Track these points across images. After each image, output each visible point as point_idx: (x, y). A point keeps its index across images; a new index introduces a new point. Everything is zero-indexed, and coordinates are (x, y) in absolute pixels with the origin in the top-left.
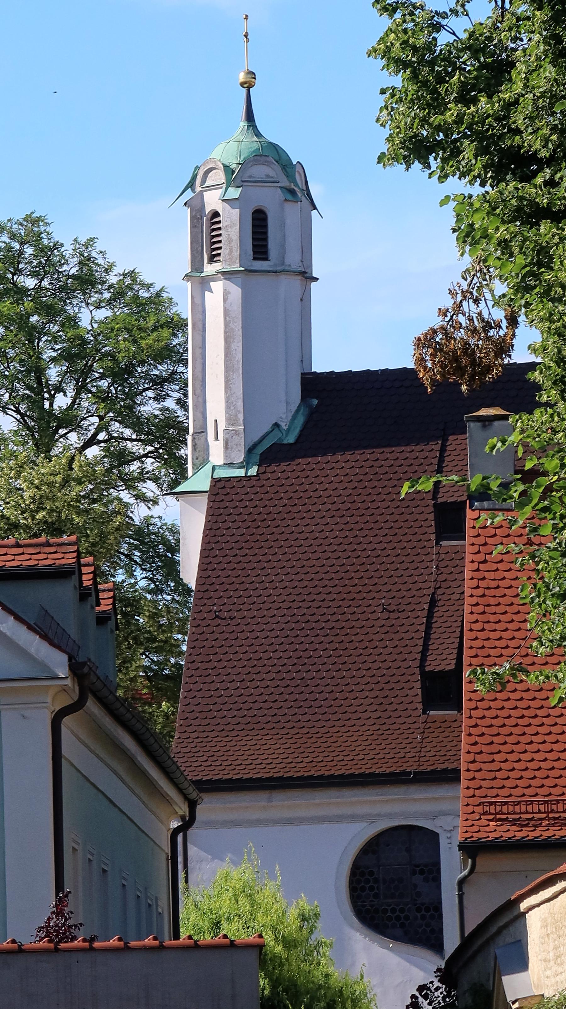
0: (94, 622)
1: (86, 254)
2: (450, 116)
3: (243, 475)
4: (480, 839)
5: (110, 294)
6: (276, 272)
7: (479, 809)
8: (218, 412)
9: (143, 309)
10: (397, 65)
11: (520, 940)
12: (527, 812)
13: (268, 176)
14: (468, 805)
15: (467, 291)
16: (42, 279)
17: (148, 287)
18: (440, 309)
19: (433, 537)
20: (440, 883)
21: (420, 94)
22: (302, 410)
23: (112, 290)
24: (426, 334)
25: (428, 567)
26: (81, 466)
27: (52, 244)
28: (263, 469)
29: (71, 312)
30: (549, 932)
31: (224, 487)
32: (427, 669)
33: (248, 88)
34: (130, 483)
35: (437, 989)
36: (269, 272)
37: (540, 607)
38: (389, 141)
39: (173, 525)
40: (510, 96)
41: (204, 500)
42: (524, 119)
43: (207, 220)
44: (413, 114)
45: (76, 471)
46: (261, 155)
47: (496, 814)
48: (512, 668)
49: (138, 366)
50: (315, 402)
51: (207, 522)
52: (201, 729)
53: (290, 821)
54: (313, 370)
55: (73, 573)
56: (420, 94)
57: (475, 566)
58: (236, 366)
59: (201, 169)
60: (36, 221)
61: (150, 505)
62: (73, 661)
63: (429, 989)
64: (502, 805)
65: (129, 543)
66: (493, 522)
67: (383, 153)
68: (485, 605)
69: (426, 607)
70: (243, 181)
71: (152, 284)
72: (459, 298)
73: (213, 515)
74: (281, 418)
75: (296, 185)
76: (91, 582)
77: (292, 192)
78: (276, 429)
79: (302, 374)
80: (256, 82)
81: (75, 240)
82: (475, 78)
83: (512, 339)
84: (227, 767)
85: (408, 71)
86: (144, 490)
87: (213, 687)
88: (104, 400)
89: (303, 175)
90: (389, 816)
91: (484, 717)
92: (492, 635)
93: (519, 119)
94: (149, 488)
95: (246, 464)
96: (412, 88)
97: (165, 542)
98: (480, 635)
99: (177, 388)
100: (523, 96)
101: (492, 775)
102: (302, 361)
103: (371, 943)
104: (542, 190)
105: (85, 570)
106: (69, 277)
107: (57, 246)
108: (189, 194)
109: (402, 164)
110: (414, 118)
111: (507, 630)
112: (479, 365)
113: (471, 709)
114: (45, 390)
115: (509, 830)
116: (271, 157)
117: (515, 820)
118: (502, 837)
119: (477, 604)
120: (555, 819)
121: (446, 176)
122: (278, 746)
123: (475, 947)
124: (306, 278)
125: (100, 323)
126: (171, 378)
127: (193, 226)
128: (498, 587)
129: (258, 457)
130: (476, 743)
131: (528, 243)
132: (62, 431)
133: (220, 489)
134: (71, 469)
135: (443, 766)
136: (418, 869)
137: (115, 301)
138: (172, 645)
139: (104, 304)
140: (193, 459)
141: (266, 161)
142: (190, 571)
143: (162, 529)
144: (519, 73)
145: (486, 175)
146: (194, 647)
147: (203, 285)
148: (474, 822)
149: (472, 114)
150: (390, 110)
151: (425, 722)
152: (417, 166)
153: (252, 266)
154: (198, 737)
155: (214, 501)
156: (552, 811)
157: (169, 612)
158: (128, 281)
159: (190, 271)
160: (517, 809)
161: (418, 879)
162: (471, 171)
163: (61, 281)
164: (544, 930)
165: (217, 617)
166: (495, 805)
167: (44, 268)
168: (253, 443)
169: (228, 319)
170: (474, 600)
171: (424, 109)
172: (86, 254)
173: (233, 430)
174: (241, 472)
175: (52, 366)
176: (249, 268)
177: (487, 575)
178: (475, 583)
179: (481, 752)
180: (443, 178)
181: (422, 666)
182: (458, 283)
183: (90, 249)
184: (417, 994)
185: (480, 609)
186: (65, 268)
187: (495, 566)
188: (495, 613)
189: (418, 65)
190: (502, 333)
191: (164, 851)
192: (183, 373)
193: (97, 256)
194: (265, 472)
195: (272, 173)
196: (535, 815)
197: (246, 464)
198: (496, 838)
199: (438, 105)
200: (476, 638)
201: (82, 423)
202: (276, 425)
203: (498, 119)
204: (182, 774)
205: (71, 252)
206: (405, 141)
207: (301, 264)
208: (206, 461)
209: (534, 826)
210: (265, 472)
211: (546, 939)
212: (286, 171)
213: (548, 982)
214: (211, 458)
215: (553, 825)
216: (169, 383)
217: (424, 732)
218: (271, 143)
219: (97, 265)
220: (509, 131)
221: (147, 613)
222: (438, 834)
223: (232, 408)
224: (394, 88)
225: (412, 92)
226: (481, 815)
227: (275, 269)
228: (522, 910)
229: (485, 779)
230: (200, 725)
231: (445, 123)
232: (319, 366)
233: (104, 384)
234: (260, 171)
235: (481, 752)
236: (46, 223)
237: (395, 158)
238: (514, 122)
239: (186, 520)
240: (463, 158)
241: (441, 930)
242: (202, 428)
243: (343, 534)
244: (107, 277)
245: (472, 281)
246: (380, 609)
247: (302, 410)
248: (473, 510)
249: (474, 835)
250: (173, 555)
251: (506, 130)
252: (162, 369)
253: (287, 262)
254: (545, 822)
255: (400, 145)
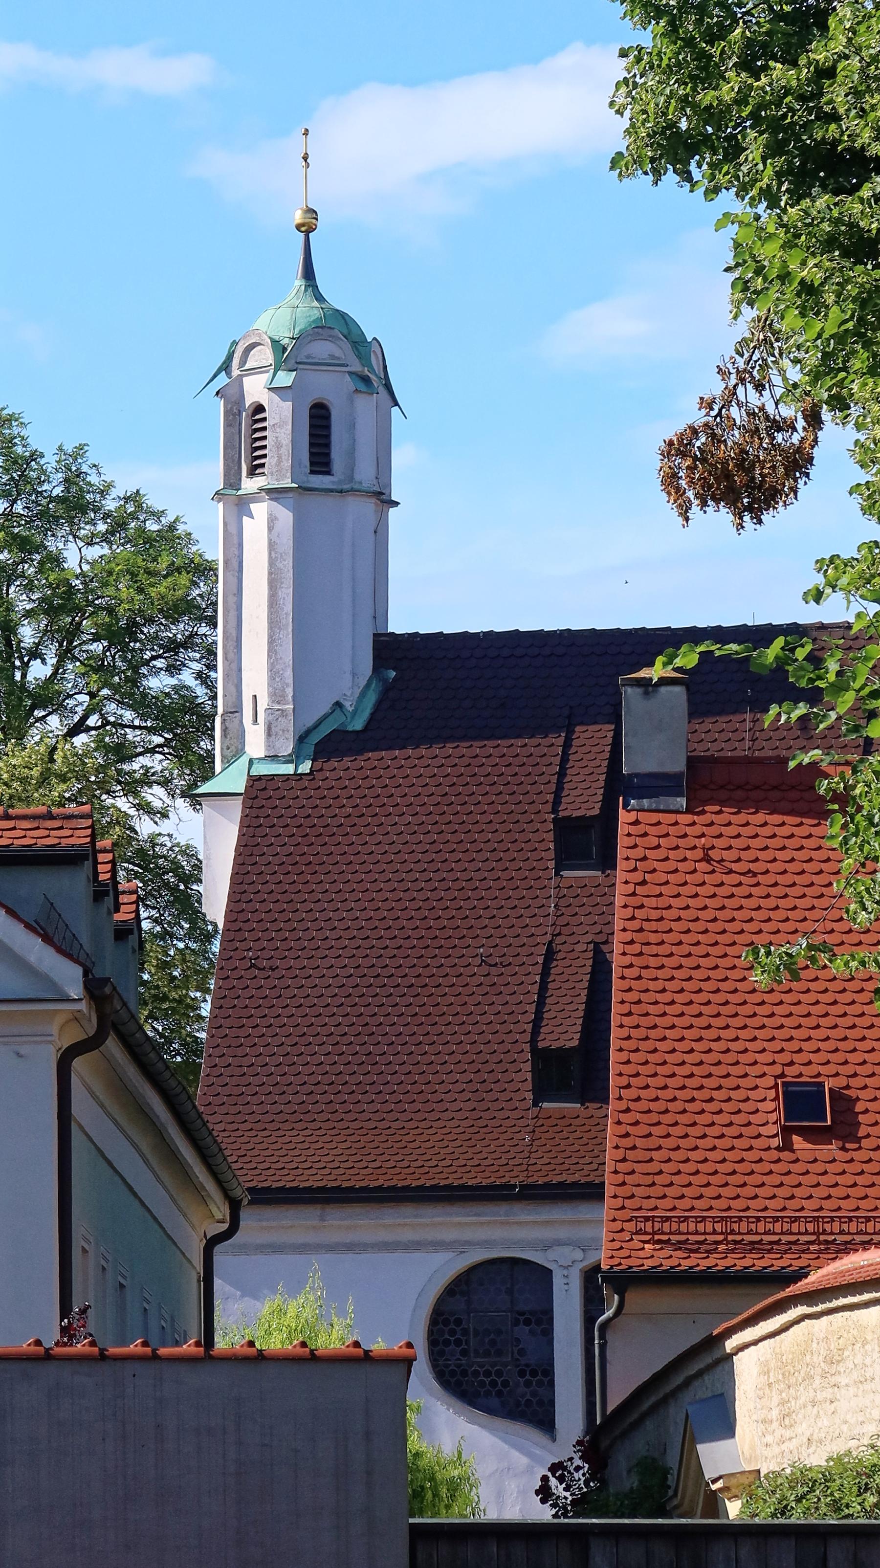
0: (111, 936)
1: (74, 469)
2: (727, 92)
3: (292, 772)
4: (631, 1267)
5: (106, 526)
6: (341, 492)
7: (630, 1226)
8: (258, 687)
9: (155, 545)
10: (646, 11)
11: (722, 1394)
12: (697, 1233)
13: (332, 357)
14: (614, 1220)
15: (745, 370)
16: (14, 502)
17: (157, 515)
18: (702, 398)
19: (551, 864)
20: (553, 1338)
21: (681, 57)
22: (373, 685)
23: (109, 521)
24: (682, 434)
25: (543, 906)
26: (65, 757)
27: (27, 454)
28: (318, 765)
29: (52, 548)
30: (771, 1381)
31: (265, 789)
32: (541, 1045)
33: (307, 233)
34: (132, 786)
35: (578, 1469)
36: (331, 491)
37: (862, 850)
38: (629, 133)
39: (188, 846)
40: (826, 58)
41: (237, 805)
42: (846, 95)
43: (247, 416)
44: (668, 91)
45: (59, 764)
46: (322, 327)
47: (654, 1233)
48: (810, 947)
49: (144, 625)
50: (393, 674)
51: (241, 835)
52: (229, 1118)
53: (350, 1248)
54: (390, 630)
55: (85, 857)
56: (681, 57)
57: (630, 888)
58: (284, 621)
59: (240, 344)
60: (7, 420)
61: (157, 819)
62: (90, 976)
63: (565, 1468)
64: (663, 1222)
65: (126, 869)
66: (789, 718)
67: (620, 154)
68: (643, 944)
69: (541, 960)
70: (297, 363)
71: (163, 512)
72: (733, 380)
73: (249, 826)
74: (345, 695)
75: (372, 371)
76: (108, 875)
77: (366, 380)
78: (338, 711)
79: (374, 634)
80: (319, 224)
81: (60, 449)
82: (767, 33)
83: (813, 447)
84: (263, 1172)
85: (662, 23)
86: (150, 798)
87: (246, 1061)
88: (96, 670)
89: (380, 356)
90: (487, 1244)
91: (638, 1099)
92: (652, 985)
93: (837, 96)
94: (156, 795)
95: (296, 757)
96: (669, 50)
97: (176, 867)
98: (635, 984)
99: (198, 656)
100: (847, 57)
101: (649, 1180)
102: (375, 617)
103: (456, 1417)
104: (871, 207)
105: (101, 857)
106: (52, 499)
107: (35, 456)
108: (223, 380)
109: (646, 173)
110: (670, 97)
111: (672, 978)
112: (760, 487)
113: (620, 1088)
114: (16, 655)
115: (671, 1257)
116: (337, 327)
117: (679, 1242)
118: (661, 1265)
119: (632, 942)
120: (735, 1242)
121: (716, 190)
122: (334, 1145)
123: (646, 1405)
124: (383, 502)
125: (92, 564)
126: (188, 643)
127: (228, 425)
128: (662, 919)
129: (313, 749)
130: (627, 1135)
131: (849, 287)
132: (39, 713)
133: (259, 789)
134: (52, 761)
135: (560, 1179)
136: (522, 1318)
137: (113, 535)
138: (188, 1006)
139: (98, 540)
140: (222, 749)
141: (330, 336)
142: (215, 899)
143: (173, 851)
144: (841, 21)
145: (779, 188)
146: (221, 1007)
147: (240, 506)
148: (624, 1245)
149: (762, 88)
150: (631, 87)
151: (537, 1117)
152: (670, 178)
153: (308, 482)
154: (225, 1130)
155: (251, 807)
156: (732, 1232)
157: (184, 961)
158: (130, 508)
159: (222, 487)
160: (683, 1227)
161: (522, 1331)
162: (756, 181)
163: (40, 505)
164: (763, 1379)
165: (253, 966)
166: (653, 1222)
167: (17, 486)
168: (305, 729)
169: (273, 555)
170: (628, 936)
171: (686, 84)
172: (74, 469)
173: (279, 710)
174: (289, 769)
175: (26, 622)
176: (304, 485)
177: (646, 901)
178: (629, 912)
179: (634, 1148)
180: (713, 191)
181: (533, 1041)
182: (732, 358)
183: (80, 461)
184: (549, 1474)
185: (636, 948)
186: (46, 487)
187: (657, 890)
188: (657, 955)
189: (679, 10)
190: (796, 439)
191: (195, 1268)
192: (206, 636)
193: (89, 472)
194: (321, 770)
195: (338, 353)
196: (708, 1237)
197: (296, 757)
198: (653, 1268)
199: (707, 73)
200: (630, 990)
201: (67, 701)
202: (338, 705)
203: (802, 98)
204: (225, 1159)
205: (54, 464)
206: (655, 133)
207: (375, 482)
208: (240, 752)
209: (707, 1252)
210: (321, 770)
211: (767, 1391)
212: (357, 349)
213: (768, 1452)
214: (247, 748)
215: (733, 1251)
216: (186, 649)
217: (534, 1131)
218: (338, 310)
219: (89, 484)
220: (818, 118)
221: (154, 962)
222: (551, 1271)
223: (278, 679)
224: (640, 49)
225: (669, 55)
226: (633, 1234)
227: (340, 487)
228: (728, 1351)
229: (639, 1185)
230: (227, 1114)
231: (720, 102)
232: (400, 623)
233: (97, 648)
234: (322, 349)
235: (634, 1148)
236: (22, 423)
237: (638, 161)
238: (831, 102)
239: (206, 835)
240: (746, 159)
241: (552, 1403)
242: (235, 707)
243: (427, 857)
244: (103, 502)
245: (751, 356)
246: (478, 961)
247: (373, 685)
248: (629, 811)
249: (622, 1261)
250: (187, 887)
251: (813, 117)
252: (178, 631)
253: (357, 477)
254: (722, 1247)
255: (647, 140)
